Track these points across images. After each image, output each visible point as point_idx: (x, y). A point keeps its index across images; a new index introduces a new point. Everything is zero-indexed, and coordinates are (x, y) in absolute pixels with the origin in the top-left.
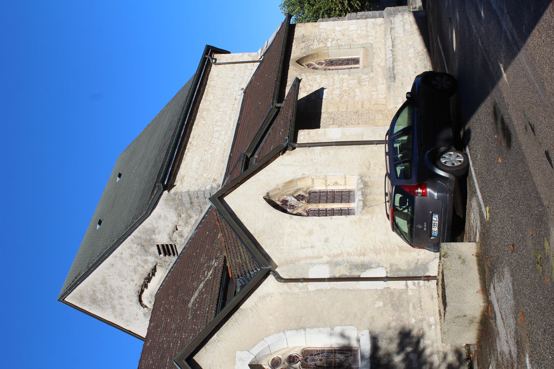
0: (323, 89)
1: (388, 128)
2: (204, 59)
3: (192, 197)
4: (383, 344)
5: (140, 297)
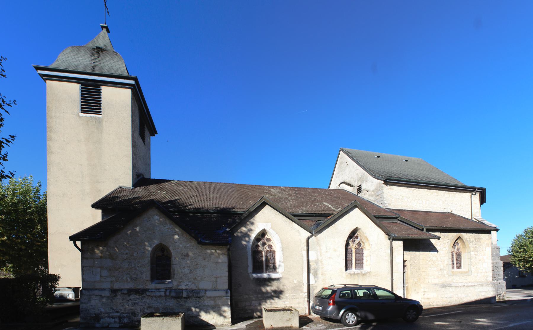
0: (437, 251)
1: (380, 286)
2: (475, 188)
3: (380, 195)
4: (275, 283)
5: (342, 183)
